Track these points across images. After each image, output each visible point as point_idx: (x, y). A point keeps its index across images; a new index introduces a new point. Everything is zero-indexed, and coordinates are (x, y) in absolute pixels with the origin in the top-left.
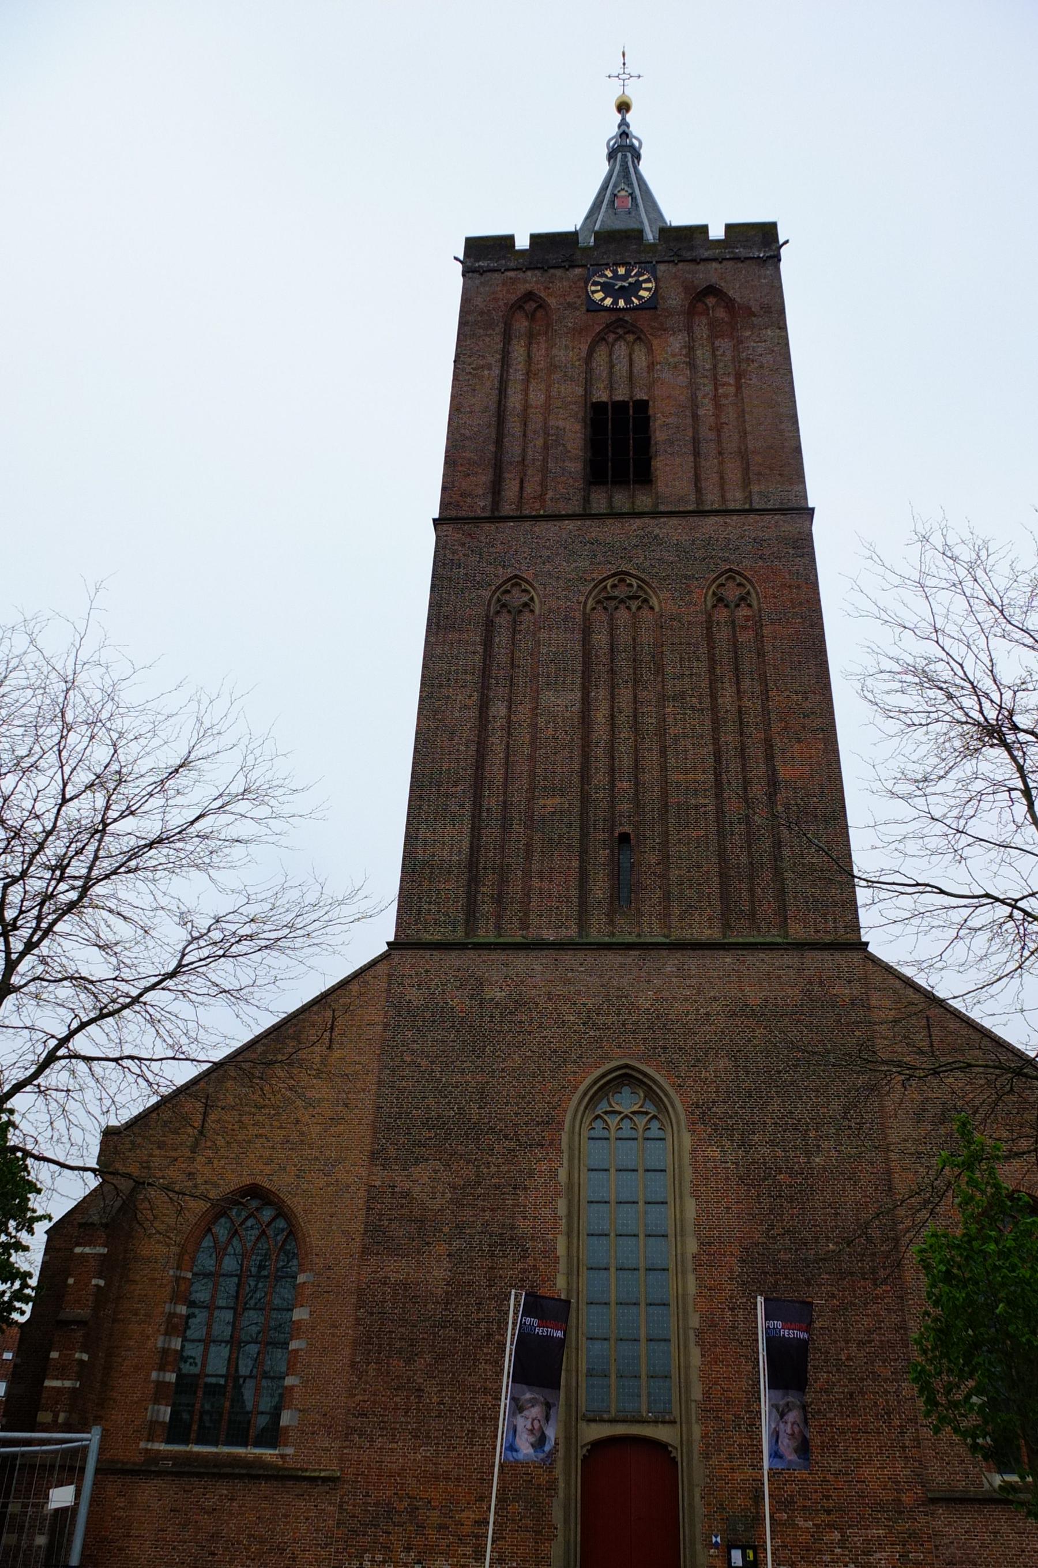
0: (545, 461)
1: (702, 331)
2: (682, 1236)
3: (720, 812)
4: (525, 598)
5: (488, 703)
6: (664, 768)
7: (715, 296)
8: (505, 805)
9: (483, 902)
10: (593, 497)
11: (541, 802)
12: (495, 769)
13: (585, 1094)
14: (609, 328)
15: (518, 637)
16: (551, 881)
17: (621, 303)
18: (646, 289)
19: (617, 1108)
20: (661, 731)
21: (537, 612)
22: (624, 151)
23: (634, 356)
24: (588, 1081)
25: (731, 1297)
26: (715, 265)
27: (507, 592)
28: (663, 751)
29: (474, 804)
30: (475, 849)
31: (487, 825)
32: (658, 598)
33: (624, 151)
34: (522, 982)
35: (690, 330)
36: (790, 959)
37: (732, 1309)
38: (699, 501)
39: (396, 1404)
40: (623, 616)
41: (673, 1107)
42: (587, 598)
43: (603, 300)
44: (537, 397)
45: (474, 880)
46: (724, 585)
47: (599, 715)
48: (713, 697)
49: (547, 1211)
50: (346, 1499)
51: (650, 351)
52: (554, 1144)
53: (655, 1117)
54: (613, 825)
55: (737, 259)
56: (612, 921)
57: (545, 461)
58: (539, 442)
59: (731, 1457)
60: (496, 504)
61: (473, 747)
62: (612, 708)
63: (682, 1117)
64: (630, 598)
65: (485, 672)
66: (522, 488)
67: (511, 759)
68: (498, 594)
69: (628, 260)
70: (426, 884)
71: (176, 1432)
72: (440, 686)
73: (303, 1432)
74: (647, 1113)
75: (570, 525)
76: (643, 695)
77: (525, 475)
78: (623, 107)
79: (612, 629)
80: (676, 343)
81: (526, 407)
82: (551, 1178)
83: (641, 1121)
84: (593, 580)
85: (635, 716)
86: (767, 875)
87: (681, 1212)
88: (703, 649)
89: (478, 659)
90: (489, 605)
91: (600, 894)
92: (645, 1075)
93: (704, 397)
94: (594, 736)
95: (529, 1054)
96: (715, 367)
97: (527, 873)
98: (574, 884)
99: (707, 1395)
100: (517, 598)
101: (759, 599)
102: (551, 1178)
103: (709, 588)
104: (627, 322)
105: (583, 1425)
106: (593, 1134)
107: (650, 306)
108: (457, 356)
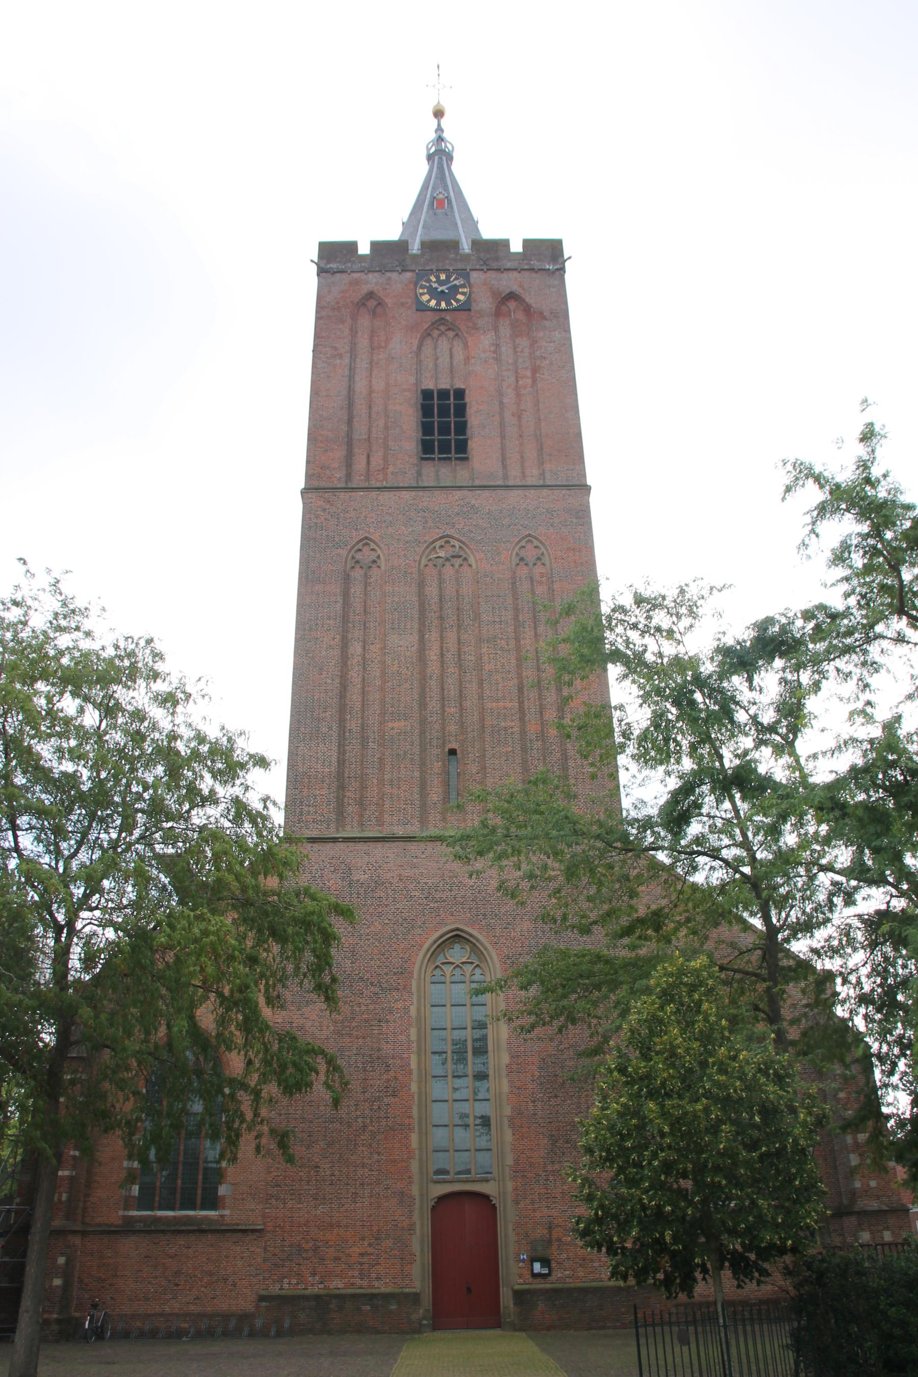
0: (386, 439)
1: (505, 330)
2: (498, 1051)
3: (523, 732)
4: (373, 556)
5: (347, 644)
6: (481, 698)
7: (516, 300)
8: (363, 728)
9: (349, 804)
10: (425, 471)
11: (390, 725)
12: (354, 697)
13: (428, 950)
14: (435, 325)
15: (369, 588)
16: (399, 788)
17: (443, 305)
18: (463, 294)
19: (451, 960)
20: (479, 667)
21: (383, 568)
22: (440, 156)
23: (454, 350)
24: (430, 941)
25: (533, 1093)
26: (515, 274)
27: (360, 550)
28: (481, 683)
29: (340, 726)
30: (341, 762)
31: (350, 743)
32: (475, 557)
33: (440, 156)
34: (380, 867)
35: (496, 329)
37: (534, 1102)
38: (506, 477)
39: (301, 1177)
40: (448, 571)
41: (491, 958)
42: (421, 557)
43: (429, 301)
44: (379, 385)
45: (342, 787)
46: (524, 547)
47: (432, 653)
48: (517, 640)
49: (404, 1037)
50: (269, 1243)
51: (466, 347)
52: (406, 988)
53: (478, 966)
54: (444, 743)
55: (532, 270)
56: (444, 818)
57: (386, 439)
58: (381, 423)
59: (533, 1202)
60: (349, 477)
61: (337, 681)
62: (442, 648)
63: (498, 966)
64: (453, 557)
65: (345, 619)
66: (368, 463)
67: (366, 689)
68: (352, 552)
69: (447, 267)
70: (306, 790)
71: (145, 1201)
72: (311, 630)
73: (235, 1199)
74: (472, 963)
75: (406, 495)
76: (464, 637)
77: (371, 450)
78: (439, 114)
79: (441, 582)
80: (487, 340)
81: (371, 392)
82: (405, 1013)
83: (468, 968)
84: (426, 542)
85: (459, 655)
87: (498, 1034)
88: (510, 600)
89: (339, 606)
90: (346, 562)
91: (435, 798)
92: (471, 935)
93: (508, 387)
94: (429, 670)
95: (387, 921)
96: (516, 362)
97: (381, 782)
98: (416, 790)
99: (516, 1161)
100: (366, 556)
101: (550, 560)
102: (405, 1013)
103: (513, 549)
104: (447, 321)
105: (431, 1185)
106: (434, 979)
107: (465, 308)
108: (315, 346)
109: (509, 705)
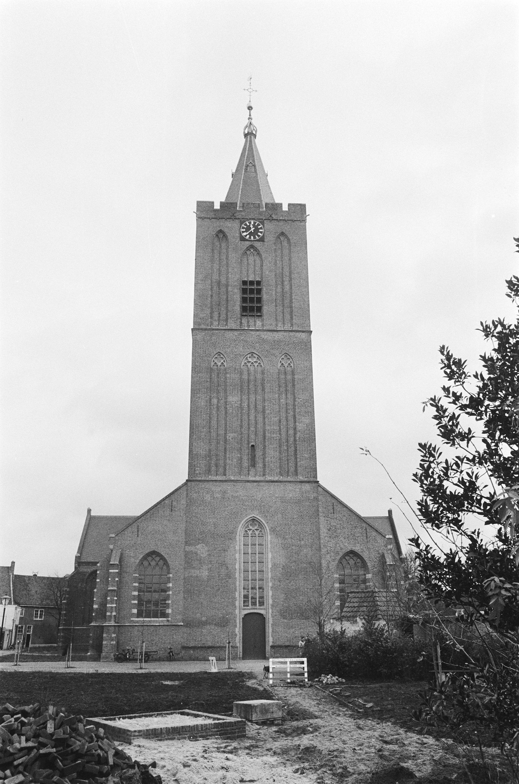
2: (242, 408)
11: (229, 435)
18: (261, 232)
20: (264, 411)
28: (264, 418)
36: (299, 486)
63: (268, 530)
75: (236, 333)
78: (250, 108)
86: (223, 408)
109: (275, 428)
